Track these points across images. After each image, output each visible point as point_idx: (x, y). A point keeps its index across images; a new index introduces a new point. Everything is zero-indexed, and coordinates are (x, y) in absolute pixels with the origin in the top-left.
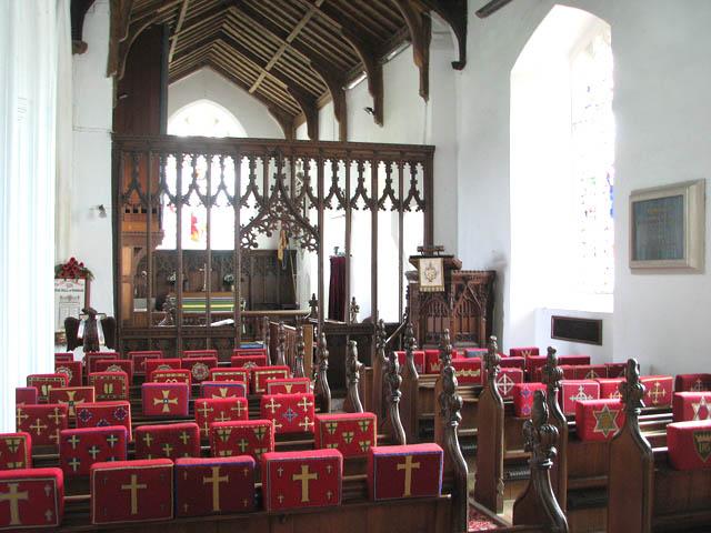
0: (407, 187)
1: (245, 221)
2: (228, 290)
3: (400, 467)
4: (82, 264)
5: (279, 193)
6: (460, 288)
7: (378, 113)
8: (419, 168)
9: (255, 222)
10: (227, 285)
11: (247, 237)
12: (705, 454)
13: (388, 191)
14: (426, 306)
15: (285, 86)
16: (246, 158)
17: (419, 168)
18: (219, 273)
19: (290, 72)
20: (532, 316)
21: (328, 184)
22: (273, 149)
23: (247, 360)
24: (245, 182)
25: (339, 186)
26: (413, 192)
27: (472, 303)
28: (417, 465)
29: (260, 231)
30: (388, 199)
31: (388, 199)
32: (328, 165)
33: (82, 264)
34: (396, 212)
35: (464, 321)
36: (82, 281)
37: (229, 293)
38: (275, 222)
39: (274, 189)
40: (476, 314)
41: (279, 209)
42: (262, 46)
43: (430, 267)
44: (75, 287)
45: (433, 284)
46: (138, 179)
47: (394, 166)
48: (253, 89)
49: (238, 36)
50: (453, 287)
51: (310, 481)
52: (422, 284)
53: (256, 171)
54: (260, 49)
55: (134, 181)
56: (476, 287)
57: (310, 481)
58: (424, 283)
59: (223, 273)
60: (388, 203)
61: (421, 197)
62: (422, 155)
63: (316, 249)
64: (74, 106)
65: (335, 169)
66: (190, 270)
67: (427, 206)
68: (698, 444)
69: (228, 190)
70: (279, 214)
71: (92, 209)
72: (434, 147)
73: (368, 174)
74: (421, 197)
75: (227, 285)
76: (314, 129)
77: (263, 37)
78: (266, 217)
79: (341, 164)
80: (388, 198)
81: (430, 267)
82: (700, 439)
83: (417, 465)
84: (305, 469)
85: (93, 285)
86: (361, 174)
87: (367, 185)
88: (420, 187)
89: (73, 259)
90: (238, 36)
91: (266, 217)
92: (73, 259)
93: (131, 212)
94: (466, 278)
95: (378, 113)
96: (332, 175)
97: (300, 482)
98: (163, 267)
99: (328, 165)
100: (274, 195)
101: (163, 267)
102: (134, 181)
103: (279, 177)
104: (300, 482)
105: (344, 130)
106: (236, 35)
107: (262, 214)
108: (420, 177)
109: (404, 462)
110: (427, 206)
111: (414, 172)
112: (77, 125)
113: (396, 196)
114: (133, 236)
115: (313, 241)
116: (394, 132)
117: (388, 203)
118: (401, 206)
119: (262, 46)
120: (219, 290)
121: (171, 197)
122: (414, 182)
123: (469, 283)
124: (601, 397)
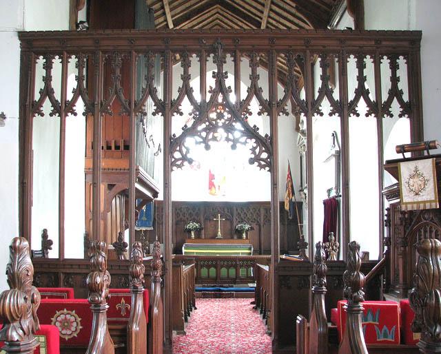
1: (176, 130)
2: (240, 237)
8: (401, 61)
9: (187, 131)
10: (239, 233)
11: (180, 151)
14: (413, 234)
16: (352, 56)
17: (401, 61)
18: (232, 223)
22: (211, 42)
23: (60, 307)
25: (367, 87)
26: (395, 92)
29: (253, 150)
30: (395, 102)
31: (395, 102)
34: (373, 119)
37: (240, 240)
38: (215, 131)
39: (214, 93)
45: (419, 199)
47: (368, 61)
52: (406, 199)
53: (366, 72)
58: (407, 197)
59: (235, 224)
60: (362, 106)
61: (406, 98)
62: (406, 44)
65: (361, 66)
66: (206, 219)
67: (413, 110)
70: (220, 123)
74: (406, 98)
75: (239, 233)
78: (204, 126)
81: (416, 174)
88: (403, 85)
91: (204, 126)
96: (53, 71)
98: (181, 216)
100: (214, 98)
101: (181, 216)
105: (359, 19)
108: (402, 73)
110: (413, 110)
111: (394, 67)
113: (372, 97)
114: (107, 172)
115: (264, 155)
117: (362, 106)
118: (379, 110)
120: (232, 238)
121: (54, 102)
122: (395, 80)
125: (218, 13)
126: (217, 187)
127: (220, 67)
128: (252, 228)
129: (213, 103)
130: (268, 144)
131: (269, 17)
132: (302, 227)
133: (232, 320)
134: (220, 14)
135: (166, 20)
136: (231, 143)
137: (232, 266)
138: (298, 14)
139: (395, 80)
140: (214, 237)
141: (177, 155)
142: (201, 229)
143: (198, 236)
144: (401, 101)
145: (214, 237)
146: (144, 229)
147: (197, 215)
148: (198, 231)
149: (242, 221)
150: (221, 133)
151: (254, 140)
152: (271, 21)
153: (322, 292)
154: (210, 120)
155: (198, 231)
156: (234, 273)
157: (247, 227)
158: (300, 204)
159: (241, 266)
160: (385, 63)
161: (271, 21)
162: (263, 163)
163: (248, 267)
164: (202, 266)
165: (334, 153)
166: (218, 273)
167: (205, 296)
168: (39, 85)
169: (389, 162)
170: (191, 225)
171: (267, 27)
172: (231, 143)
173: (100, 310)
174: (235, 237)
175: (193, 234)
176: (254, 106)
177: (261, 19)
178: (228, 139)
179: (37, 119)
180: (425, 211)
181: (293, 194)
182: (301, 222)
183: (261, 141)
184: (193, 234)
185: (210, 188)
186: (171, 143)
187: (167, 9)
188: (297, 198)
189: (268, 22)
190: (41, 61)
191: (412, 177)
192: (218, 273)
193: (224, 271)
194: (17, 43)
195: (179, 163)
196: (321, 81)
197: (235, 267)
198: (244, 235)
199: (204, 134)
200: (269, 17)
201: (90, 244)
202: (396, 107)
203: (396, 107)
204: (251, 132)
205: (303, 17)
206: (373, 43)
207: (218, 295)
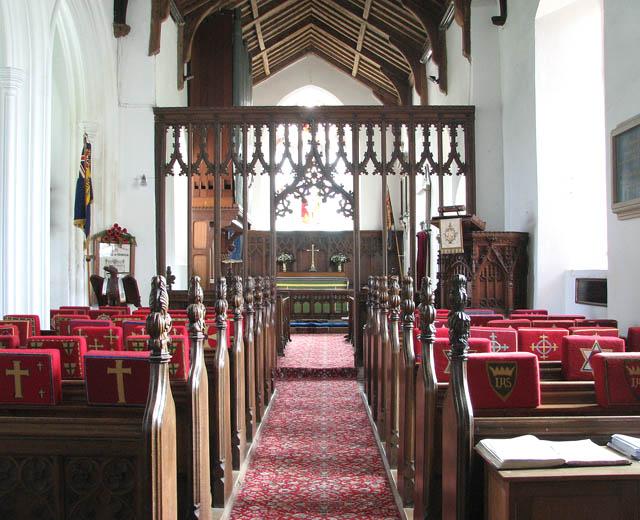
0: (447, 150)
2: (335, 270)
3: (110, 371)
4: (125, 230)
5: (314, 159)
6: (484, 251)
7: (444, 87)
8: (460, 129)
11: (348, 211)
12: (503, 391)
13: (370, 154)
15: (378, 66)
17: (460, 129)
18: (326, 254)
19: (379, 51)
20: (563, 277)
21: (419, 149)
24: (363, 149)
26: (454, 155)
27: (496, 265)
28: (128, 371)
29: (296, 197)
32: (363, 129)
33: (125, 230)
34: (378, 176)
35: (490, 286)
36: (128, 246)
39: (309, 157)
40: (503, 278)
41: (314, 175)
42: (348, 27)
43: (450, 228)
44: (121, 251)
45: (451, 246)
46: (205, 149)
47: (433, 129)
48: (268, 72)
49: (327, 19)
50: (476, 250)
51: (23, 377)
53: (374, 139)
54: (344, 28)
55: (202, 151)
56: (502, 249)
57: (23, 377)
59: (329, 256)
61: (463, 159)
63: (352, 214)
64: (119, 85)
65: (426, 134)
66: (298, 250)
67: (468, 169)
68: (493, 378)
69: (293, 157)
70: (314, 181)
71: (136, 179)
72: (474, 107)
73: (405, 138)
74: (463, 159)
75: (334, 265)
76: (425, 96)
77: (344, 16)
78: (300, 183)
79: (433, 129)
80: (427, 162)
81: (450, 228)
82: (496, 372)
83: (128, 371)
84: (17, 364)
85: (138, 250)
86: (427, 139)
87: (433, 149)
88: (461, 150)
89: (116, 225)
90: (327, 19)
91: (300, 183)
92: (116, 225)
93: (207, 187)
94: (489, 240)
95: (444, 87)
97: (13, 377)
99: (419, 130)
102: (202, 151)
103: (314, 144)
104: (13, 377)
106: (325, 18)
107: (297, 180)
109: (114, 366)
111: (453, 134)
112: (123, 101)
115: (349, 207)
116: (454, 98)
117: (370, 167)
119: (348, 27)
120: (327, 271)
121: (182, 164)
123: (494, 245)
124: (519, 350)
125: (311, 12)
126: (310, 214)
127: (314, 135)
128: (348, 260)
129: (309, 164)
130: (352, 198)
131: (364, 40)
132: (402, 258)
133: (325, 348)
134: (316, 22)
135: (258, 43)
136: (322, 197)
137: (305, 300)
138: (392, 46)
139: (454, 145)
140: (307, 270)
141: (280, 207)
142: (293, 261)
143: (290, 269)
144: (458, 162)
145: (307, 270)
146: (232, 261)
147: (290, 246)
148: (290, 264)
149: (337, 253)
150: (314, 190)
151: (340, 195)
152: (374, 9)
153: (395, 320)
154: (306, 179)
155: (290, 264)
156: (200, 257)
157: (343, 259)
158: (401, 234)
159: (336, 300)
160: (446, 131)
161: (374, 9)
162: (348, 213)
163: (343, 301)
164: (295, 301)
165: (425, 187)
166: (312, 308)
167: (299, 331)
168: (170, 151)
169: (434, 219)
170: (283, 257)
171: (363, 48)
172: (322, 197)
173: (161, 359)
174: (330, 269)
175: (284, 266)
176: (341, 166)
177: (360, 25)
178: (320, 194)
179: (168, 178)
180: (457, 255)
181: (393, 222)
182: (402, 253)
183: (346, 196)
184: (284, 266)
185: (303, 216)
186: (276, 199)
187: (260, 36)
188: (396, 226)
189: (371, 10)
190: (171, 131)
191: (447, 230)
192: (312, 308)
193: (318, 306)
194: (151, 117)
195: (281, 213)
196: (402, 140)
197: (329, 301)
198: (340, 268)
199: (301, 190)
200: (364, 40)
201: (192, 282)
202: (454, 167)
203: (454, 167)
204: (338, 189)
205: (398, 50)
206: (436, 115)
207: (312, 330)
